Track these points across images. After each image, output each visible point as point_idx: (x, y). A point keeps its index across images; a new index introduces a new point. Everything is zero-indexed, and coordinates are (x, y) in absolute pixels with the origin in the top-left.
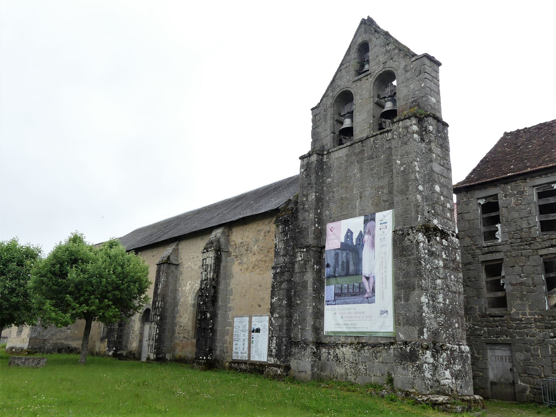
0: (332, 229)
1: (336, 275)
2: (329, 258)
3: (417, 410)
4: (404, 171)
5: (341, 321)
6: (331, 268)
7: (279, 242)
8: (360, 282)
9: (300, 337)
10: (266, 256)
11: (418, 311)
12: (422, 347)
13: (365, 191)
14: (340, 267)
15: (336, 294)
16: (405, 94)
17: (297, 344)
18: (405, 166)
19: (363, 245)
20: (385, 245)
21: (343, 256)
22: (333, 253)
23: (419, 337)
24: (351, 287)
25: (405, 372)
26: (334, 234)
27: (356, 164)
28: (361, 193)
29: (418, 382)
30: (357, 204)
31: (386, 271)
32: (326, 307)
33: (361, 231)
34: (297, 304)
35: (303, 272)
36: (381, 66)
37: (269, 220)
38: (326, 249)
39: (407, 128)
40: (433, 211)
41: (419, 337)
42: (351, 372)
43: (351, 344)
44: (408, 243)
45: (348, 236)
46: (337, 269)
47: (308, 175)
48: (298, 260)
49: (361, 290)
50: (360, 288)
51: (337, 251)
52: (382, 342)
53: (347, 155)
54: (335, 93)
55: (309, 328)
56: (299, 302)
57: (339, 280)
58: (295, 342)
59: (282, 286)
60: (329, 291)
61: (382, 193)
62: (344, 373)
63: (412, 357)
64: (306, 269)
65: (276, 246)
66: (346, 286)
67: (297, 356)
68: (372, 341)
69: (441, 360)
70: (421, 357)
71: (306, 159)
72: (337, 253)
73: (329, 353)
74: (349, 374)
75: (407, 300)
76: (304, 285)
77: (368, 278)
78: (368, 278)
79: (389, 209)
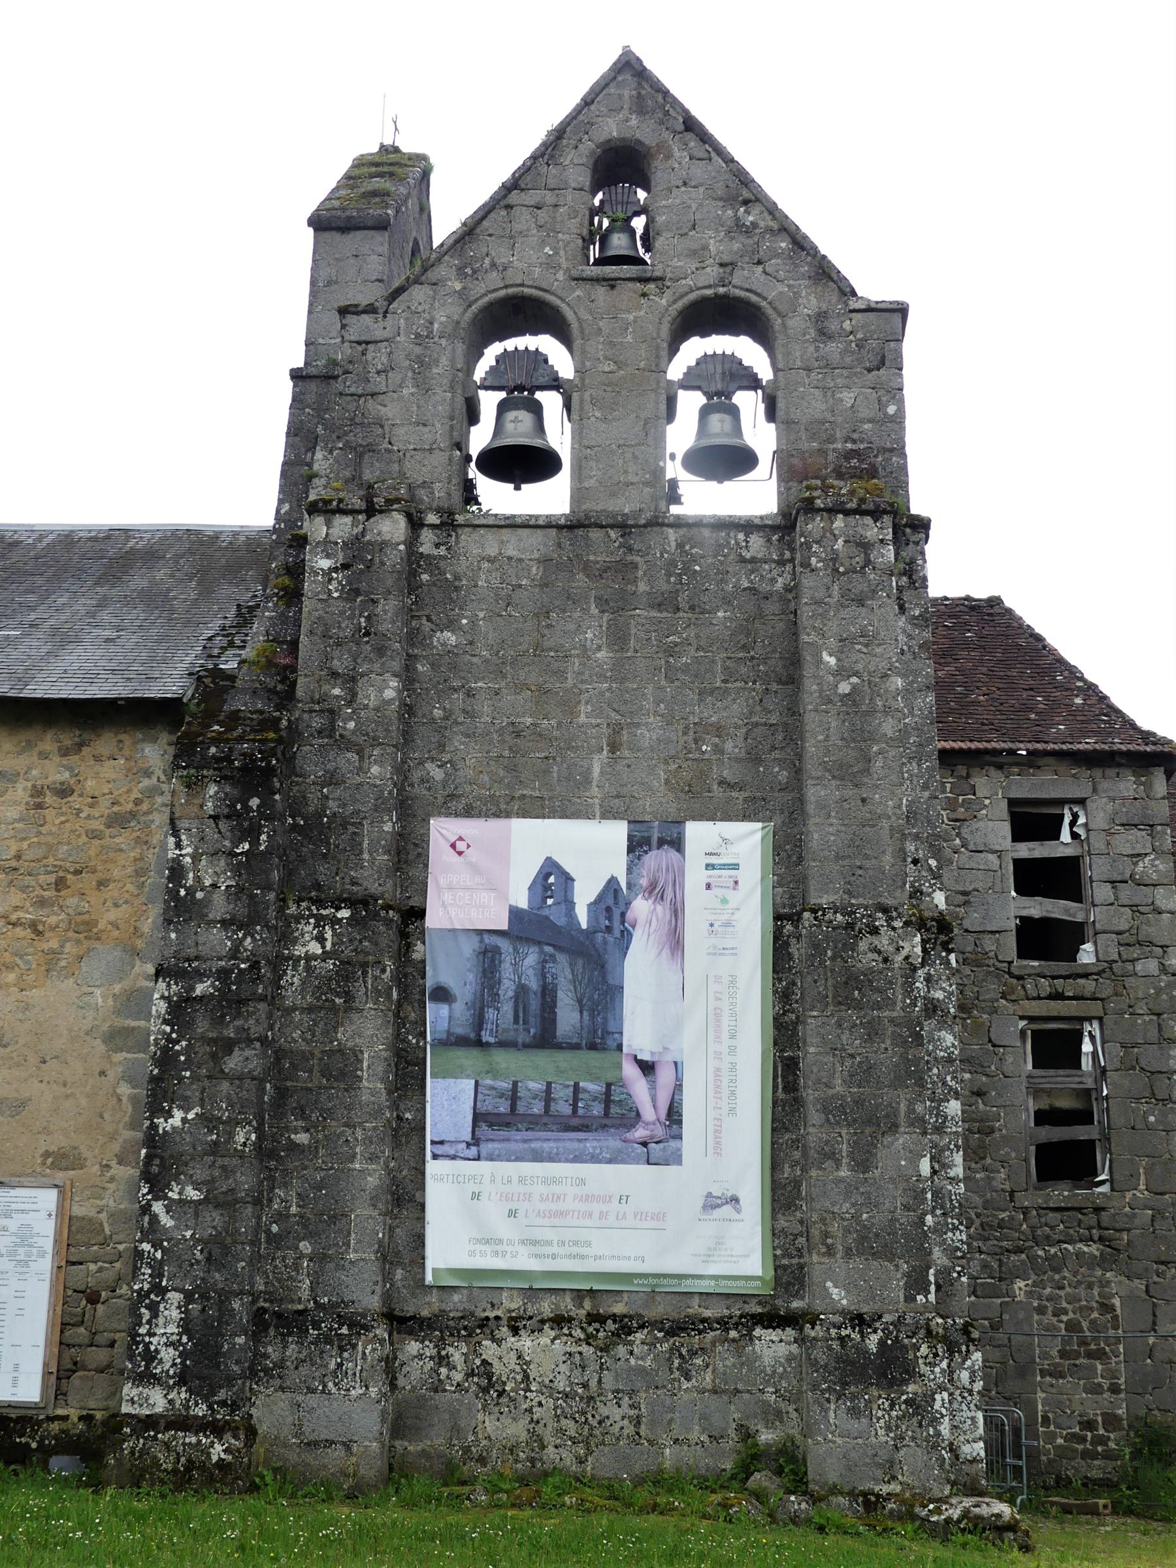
0: (461, 846)
1: (486, 1037)
2: (448, 966)
3: (933, 1550)
4: (851, 698)
5: (505, 1229)
6: (459, 1007)
7: (196, 857)
8: (610, 1077)
9: (305, 1294)
10: (41, 903)
11: (907, 1208)
12: (929, 1333)
13: (638, 725)
14: (507, 1008)
15: (478, 1118)
16: (818, 416)
17: (293, 1323)
18: (854, 680)
19: (626, 937)
20: (733, 951)
21: (522, 967)
22: (469, 947)
23: (910, 1299)
24: (562, 1094)
25: (855, 1425)
26: (475, 868)
27: (594, 610)
28: (616, 729)
29: (912, 1458)
30: (596, 770)
31: (732, 1050)
32: (432, 1168)
33: (613, 881)
34: (293, 1147)
35: (334, 1009)
36: (712, 272)
37: (68, 739)
38: (433, 920)
39: (865, 546)
40: (933, 863)
41: (910, 1299)
42: (562, 1431)
43: (560, 1321)
44: (868, 960)
45: (547, 887)
46: (490, 1014)
47: (357, 592)
48: (299, 951)
49: (614, 1110)
50: (607, 1100)
51: (488, 939)
52: (707, 1313)
53: (545, 561)
54: (481, 288)
55: (360, 1255)
56: (302, 1138)
57: (503, 1059)
58: (279, 1315)
59: (233, 1063)
60: (448, 1101)
61: (718, 750)
62: (524, 1436)
63: (892, 1368)
64: (349, 997)
65: (176, 871)
66: (536, 1086)
67: (294, 1377)
68: (657, 1311)
69: (965, 1376)
70: (924, 1369)
71: (348, 520)
72: (488, 952)
73: (442, 1360)
74: (549, 1439)
75: (863, 1161)
76: (341, 1068)
77: (647, 1068)
78: (647, 1068)
79: (745, 818)
